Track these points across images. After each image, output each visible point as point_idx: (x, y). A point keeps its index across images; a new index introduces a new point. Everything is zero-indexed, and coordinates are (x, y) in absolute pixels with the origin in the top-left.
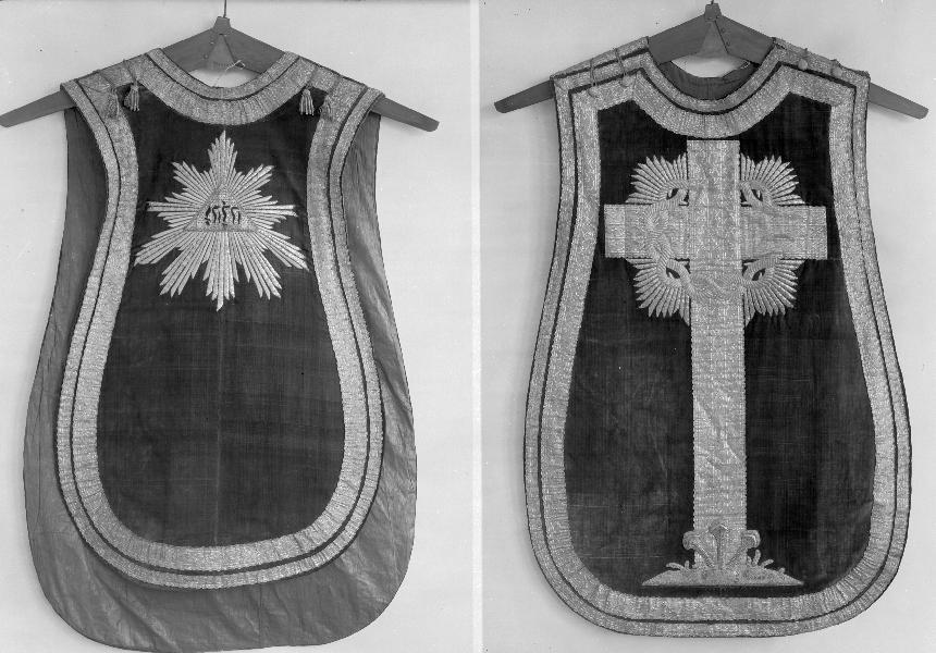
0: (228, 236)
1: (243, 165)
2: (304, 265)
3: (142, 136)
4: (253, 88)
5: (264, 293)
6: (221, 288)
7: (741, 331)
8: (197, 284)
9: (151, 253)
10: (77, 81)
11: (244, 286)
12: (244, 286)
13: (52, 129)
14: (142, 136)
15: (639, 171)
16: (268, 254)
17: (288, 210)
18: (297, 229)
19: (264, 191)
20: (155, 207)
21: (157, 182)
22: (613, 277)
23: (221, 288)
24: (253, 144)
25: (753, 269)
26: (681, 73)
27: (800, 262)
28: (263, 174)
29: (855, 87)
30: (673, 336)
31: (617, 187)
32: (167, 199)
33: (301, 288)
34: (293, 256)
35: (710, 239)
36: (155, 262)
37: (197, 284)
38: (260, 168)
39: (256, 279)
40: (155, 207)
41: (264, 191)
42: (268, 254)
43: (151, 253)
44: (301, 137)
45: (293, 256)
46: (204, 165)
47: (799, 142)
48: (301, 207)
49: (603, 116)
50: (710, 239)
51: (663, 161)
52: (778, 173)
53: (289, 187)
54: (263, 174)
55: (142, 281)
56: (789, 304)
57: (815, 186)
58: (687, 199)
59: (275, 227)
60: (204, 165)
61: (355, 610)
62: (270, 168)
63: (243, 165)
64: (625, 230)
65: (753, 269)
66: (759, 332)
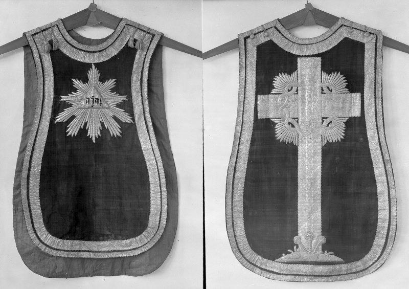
0: (92, 110)
1: (102, 80)
2: (131, 121)
3: (58, 64)
4: (330, 33)
5: (113, 134)
6: (94, 132)
7: (320, 151)
8: (83, 131)
9: (61, 117)
10: (162, 36)
11: (104, 130)
12: (104, 130)
13: (18, 60)
14: (58, 64)
15: (275, 79)
16: (115, 118)
17: (123, 98)
18: (128, 106)
19: (112, 90)
20: (64, 98)
21: (63, 85)
22: (264, 128)
23: (94, 132)
24: (107, 70)
25: (294, 122)
26: (101, 25)
27: (347, 119)
28: (111, 83)
29: (342, 25)
30: (290, 152)
31: (264, 87)
32: (73, 93)
33: (129, 130)
34: (125, 118)
35: (310, 111)
36: (65, 121)
37: (83, 131)
38: (110, 80)
39: (109, 128)
40: (64, 98)
41: (112, 90)
42: (115, 118)
43: (61, 117)
44: (133, 63)
45: (125, 118)
46: (85, 80)
47: (348, 61)
48: (129, 95)
49: (259, 48)
50: (310, 111)
51: (286, 74)
52: (337, 80)
53: (123, 87)
54: (111, 83)
55: (57, 130)
56: (343, 138)
57: (355, 84)
58: (297, 91)
59: (118, 106)
60: (85, 80)
61: (76, 222)
62: (114, 80)
63: (102, 80)
64: (270, 106)
65: (294, 122)
66: (328, 150)
